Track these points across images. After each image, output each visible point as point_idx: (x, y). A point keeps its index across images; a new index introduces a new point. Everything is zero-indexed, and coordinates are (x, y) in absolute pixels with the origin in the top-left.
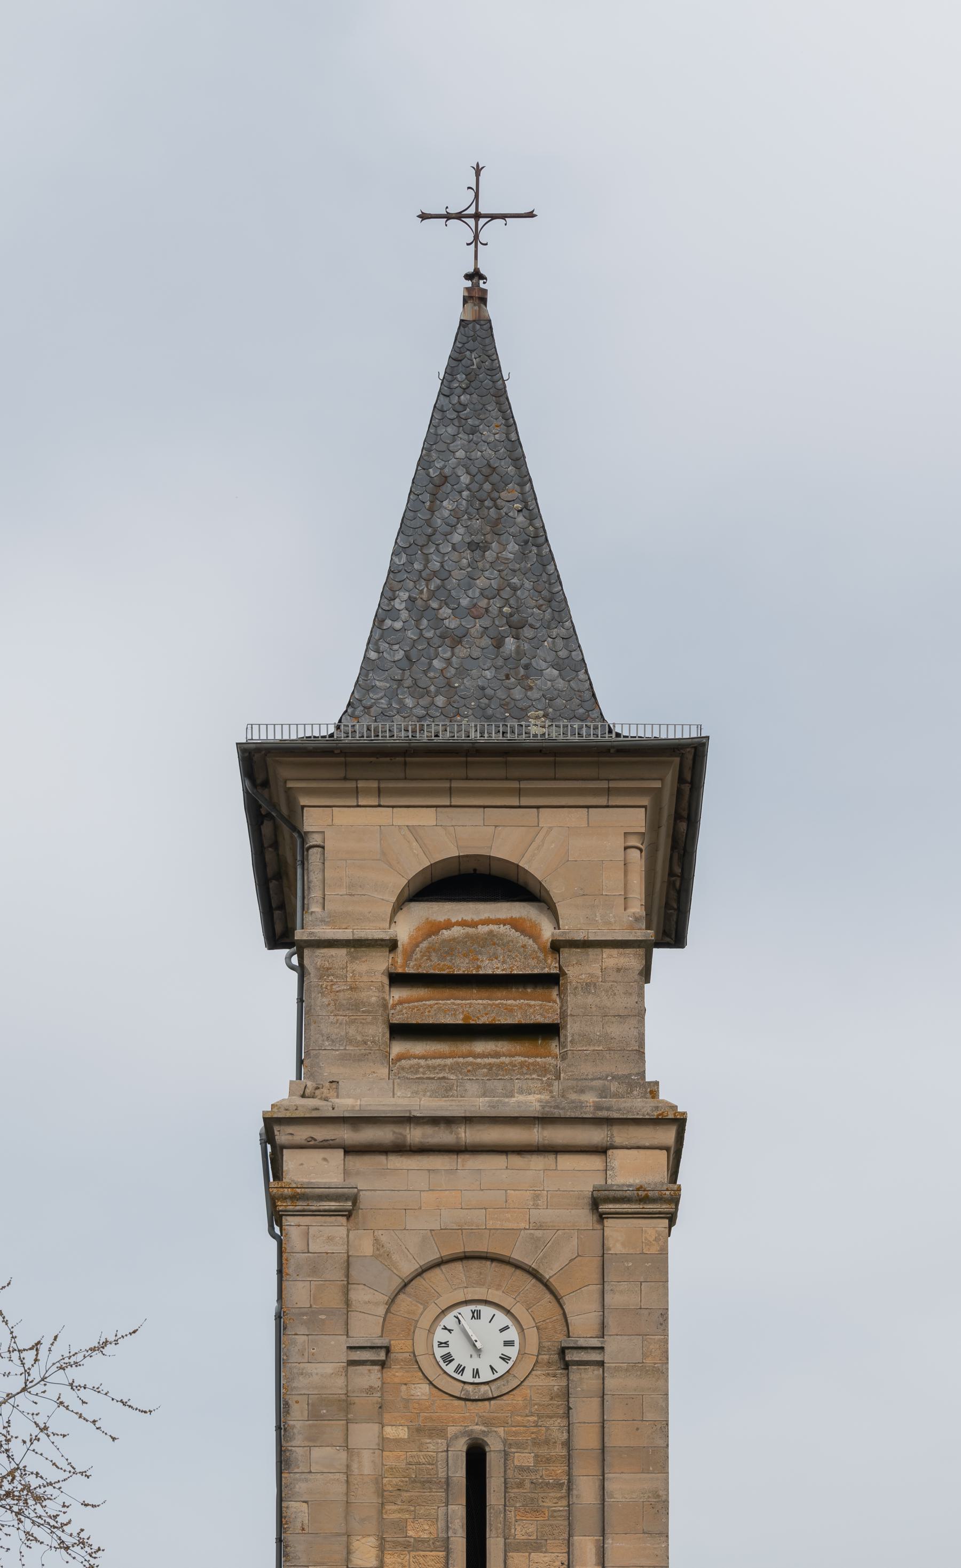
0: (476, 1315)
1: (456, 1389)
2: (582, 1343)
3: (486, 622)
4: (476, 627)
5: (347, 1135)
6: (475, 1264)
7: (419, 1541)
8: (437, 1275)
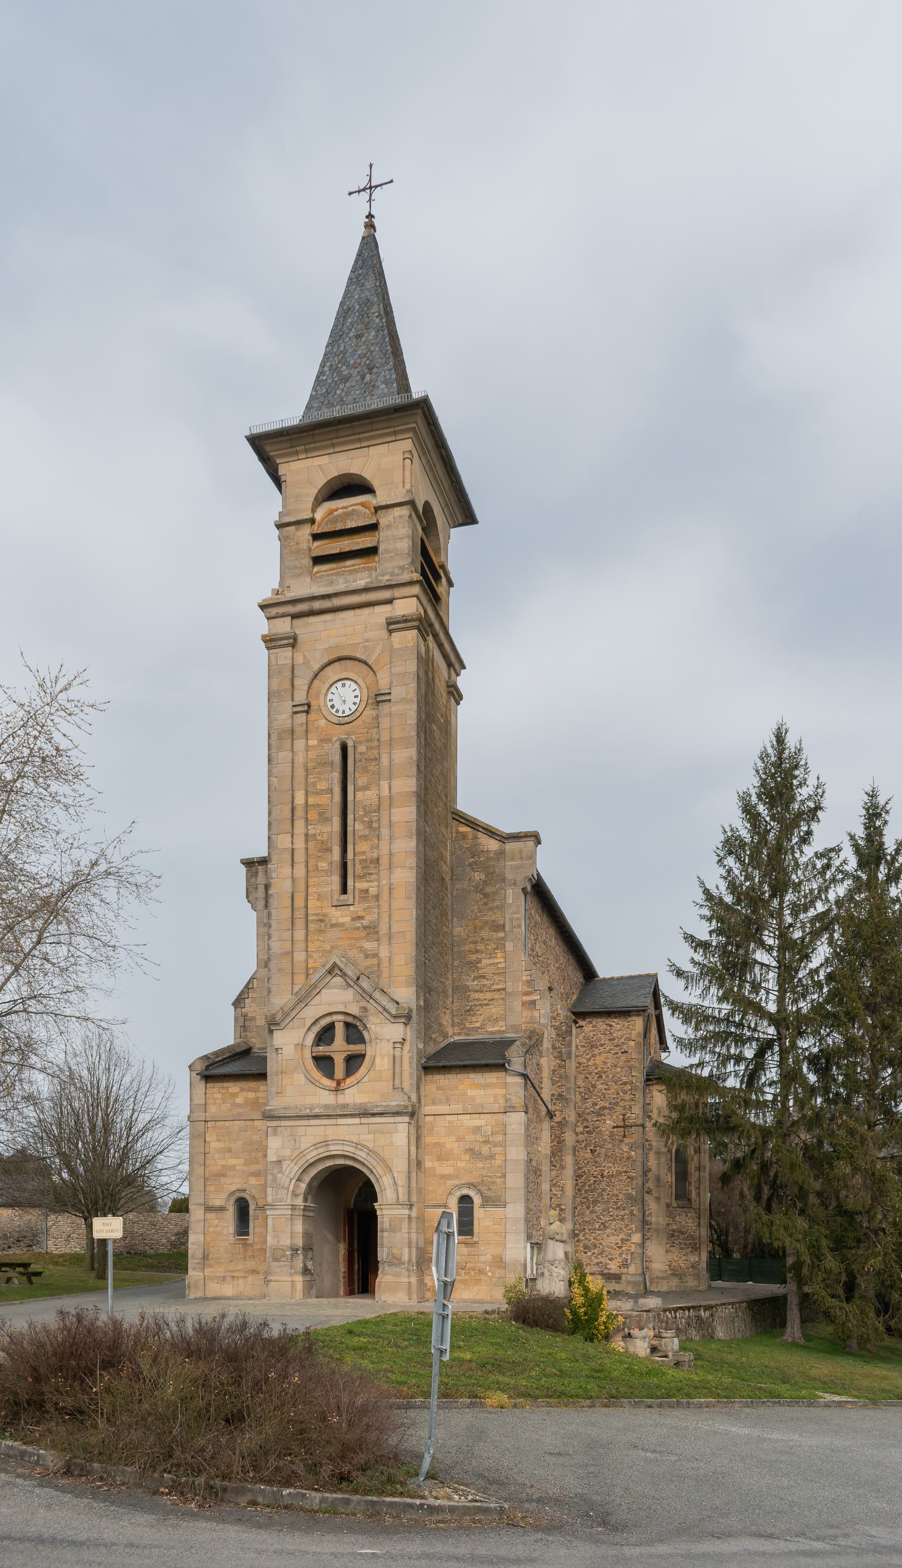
0: (344, 685)
1: (335, 720)
2: (382, 692)
3: (359, 369)
4: (355, 372)
5: (291, 609)
6: (343, 662)
7: (322, 790)
8: (329, 669)
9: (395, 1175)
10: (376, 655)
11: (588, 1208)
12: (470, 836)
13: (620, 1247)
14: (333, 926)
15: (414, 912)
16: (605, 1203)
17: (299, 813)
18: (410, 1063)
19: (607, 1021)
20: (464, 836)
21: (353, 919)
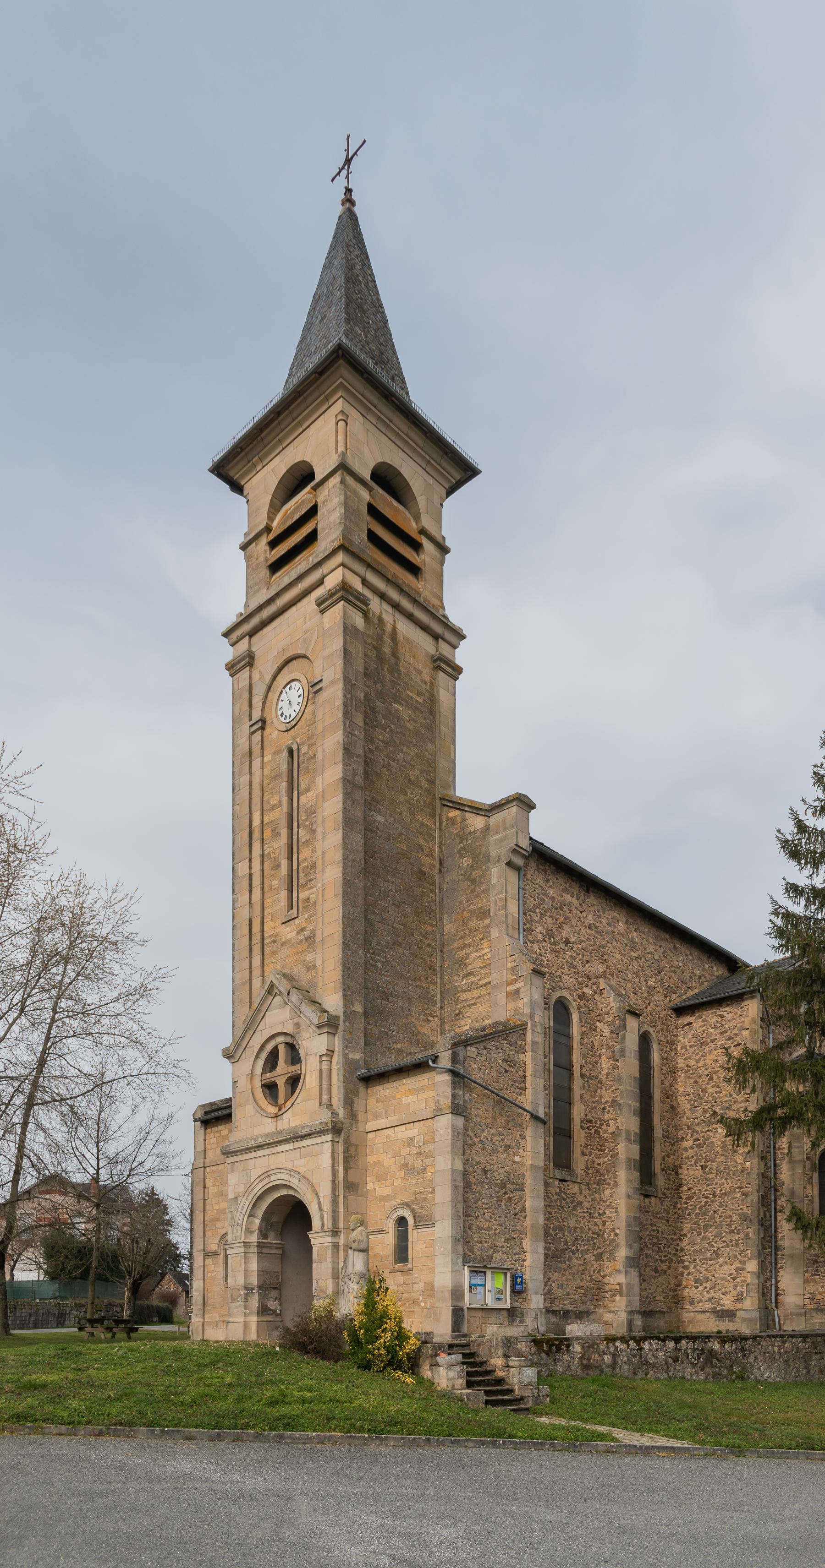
6: (291, 664)
7: (274, 805)
9: (322, 1201)
10: (313, 643)
11: (699, 1234)
12: (459, 820)
13: (734, 1279)
16: (717, 1227)
17: (256, 835)
18: (338, 1075)
19: (719, 1012)
20: (453, 821)
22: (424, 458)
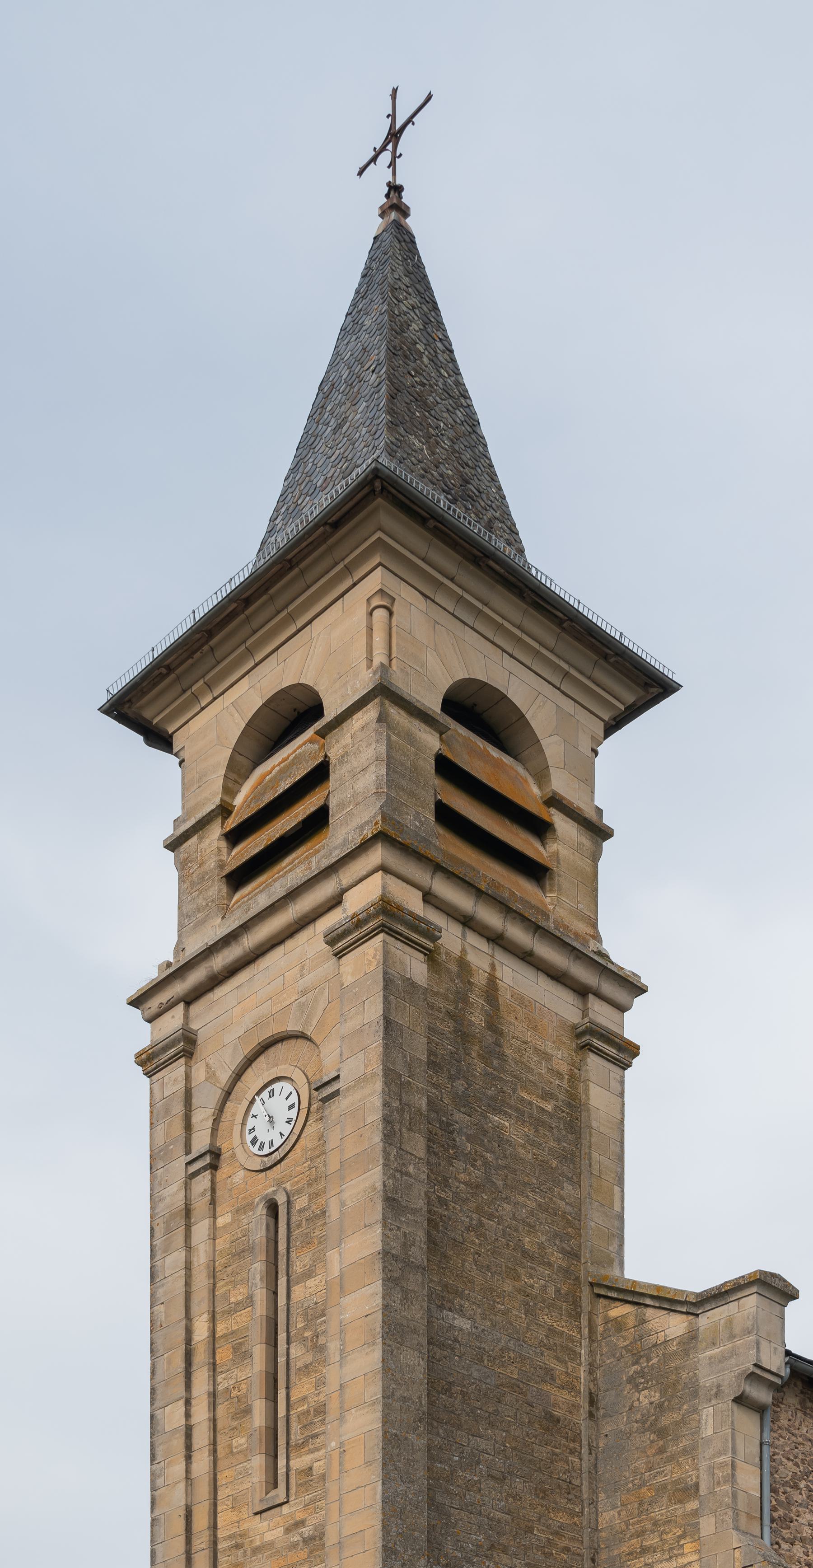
1: (257, 1164)
6: (272, 1050)
7: (237, 1304)
12: (631, 1322)
14: (256, 1551)
15: (379, 1488)
17: (201, 1357)
20: (619, 1325)
21: (288, 1530)
22: (556, 667)
